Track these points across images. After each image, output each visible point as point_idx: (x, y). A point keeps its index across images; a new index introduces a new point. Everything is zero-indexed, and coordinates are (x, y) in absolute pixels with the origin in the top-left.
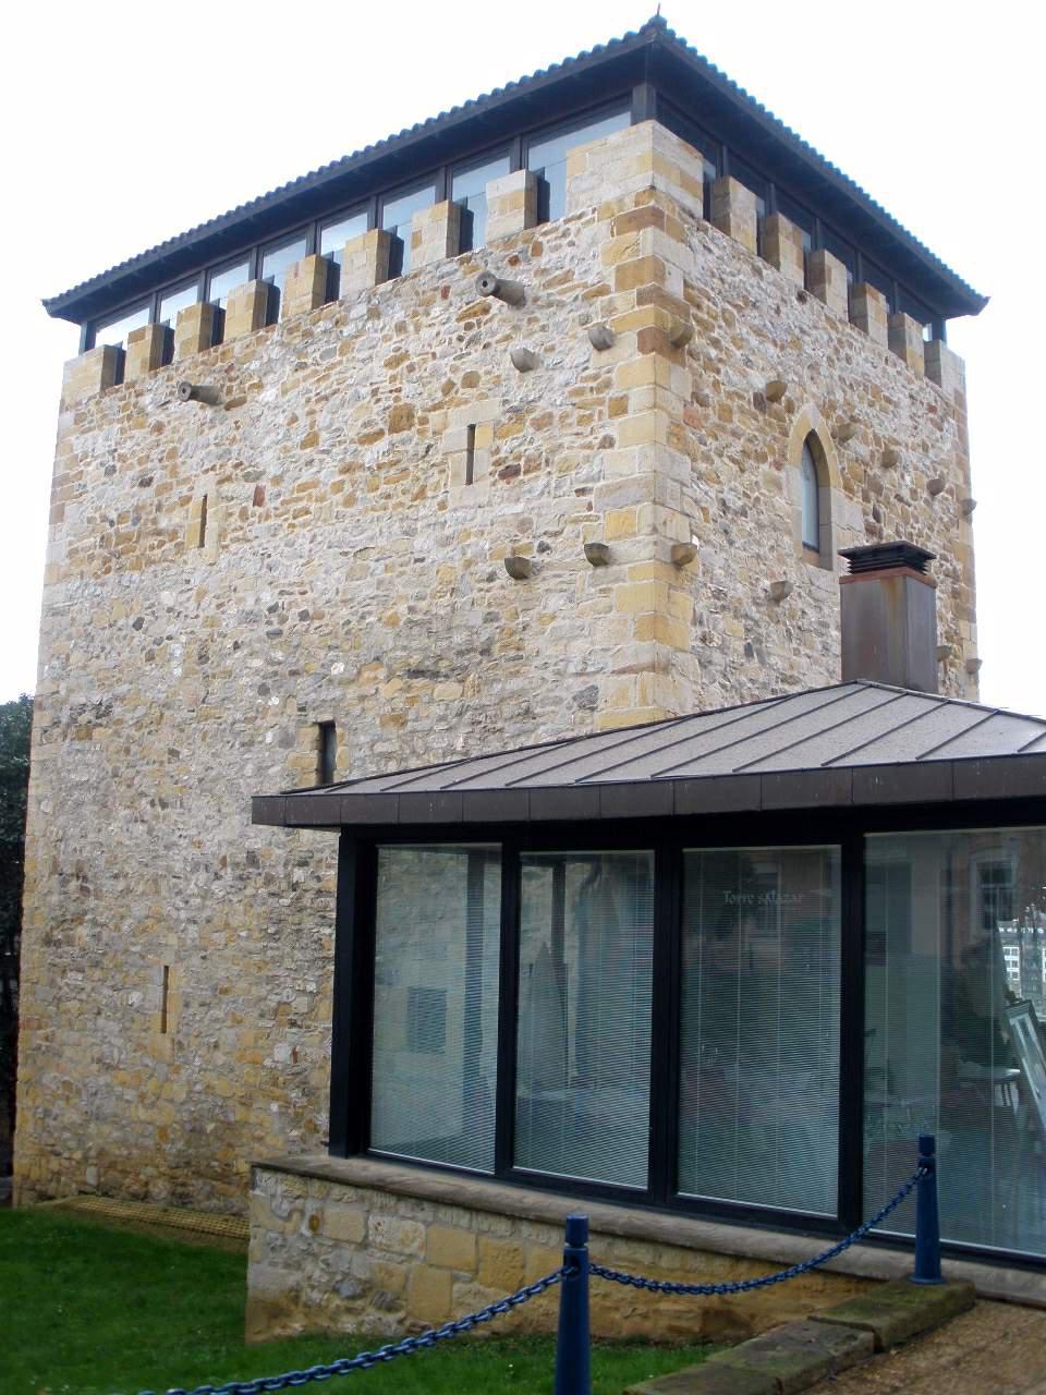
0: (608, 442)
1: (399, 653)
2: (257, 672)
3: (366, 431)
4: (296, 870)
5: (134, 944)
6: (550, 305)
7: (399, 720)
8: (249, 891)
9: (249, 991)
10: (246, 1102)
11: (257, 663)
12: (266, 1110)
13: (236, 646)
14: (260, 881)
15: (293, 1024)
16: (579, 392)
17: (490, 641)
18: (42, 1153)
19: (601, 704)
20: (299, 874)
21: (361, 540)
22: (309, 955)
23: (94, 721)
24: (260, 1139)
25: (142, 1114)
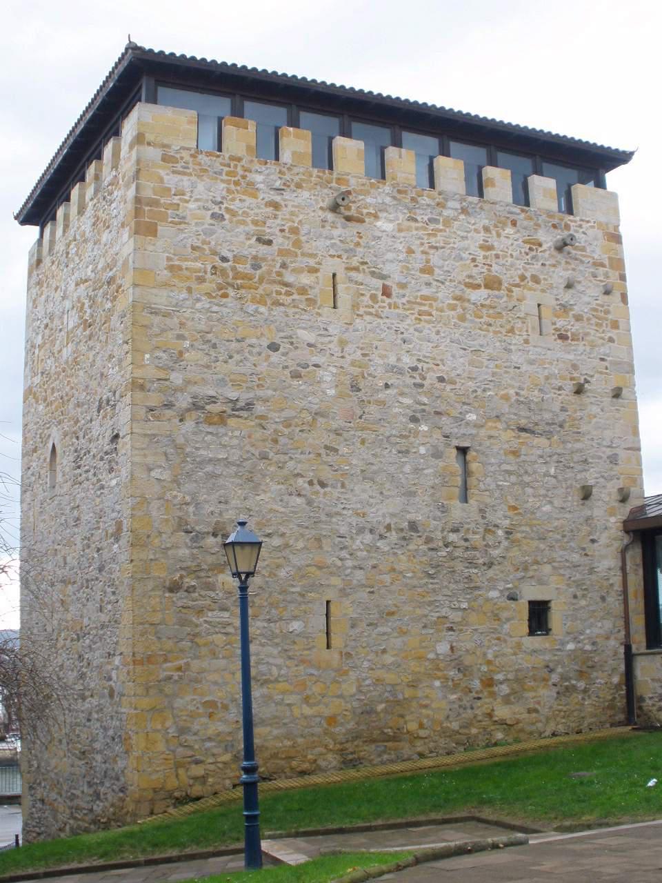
0: (611, 340)
1: (512, 416)
2: (408, 407)
3: (467, 280)
4: (451, 534)
5: (293, 586)
6: (576, 259)
7: (515, 453)
8: (412, 547)
9: (414, 612)
10: (413, 685)
11: (407, 401)
12: (431, 687)
13: (387, 386)
14: (420, 541)
15: (451, 629)
16: (596, 310)
17: (564, 421)
18: (178, 765)
19: (620, 462)
20: (453, 537)
21: (475, 344)
22: (461, 586)
23: (229, 412)
24: (426, 706)
25: (307, 711)
